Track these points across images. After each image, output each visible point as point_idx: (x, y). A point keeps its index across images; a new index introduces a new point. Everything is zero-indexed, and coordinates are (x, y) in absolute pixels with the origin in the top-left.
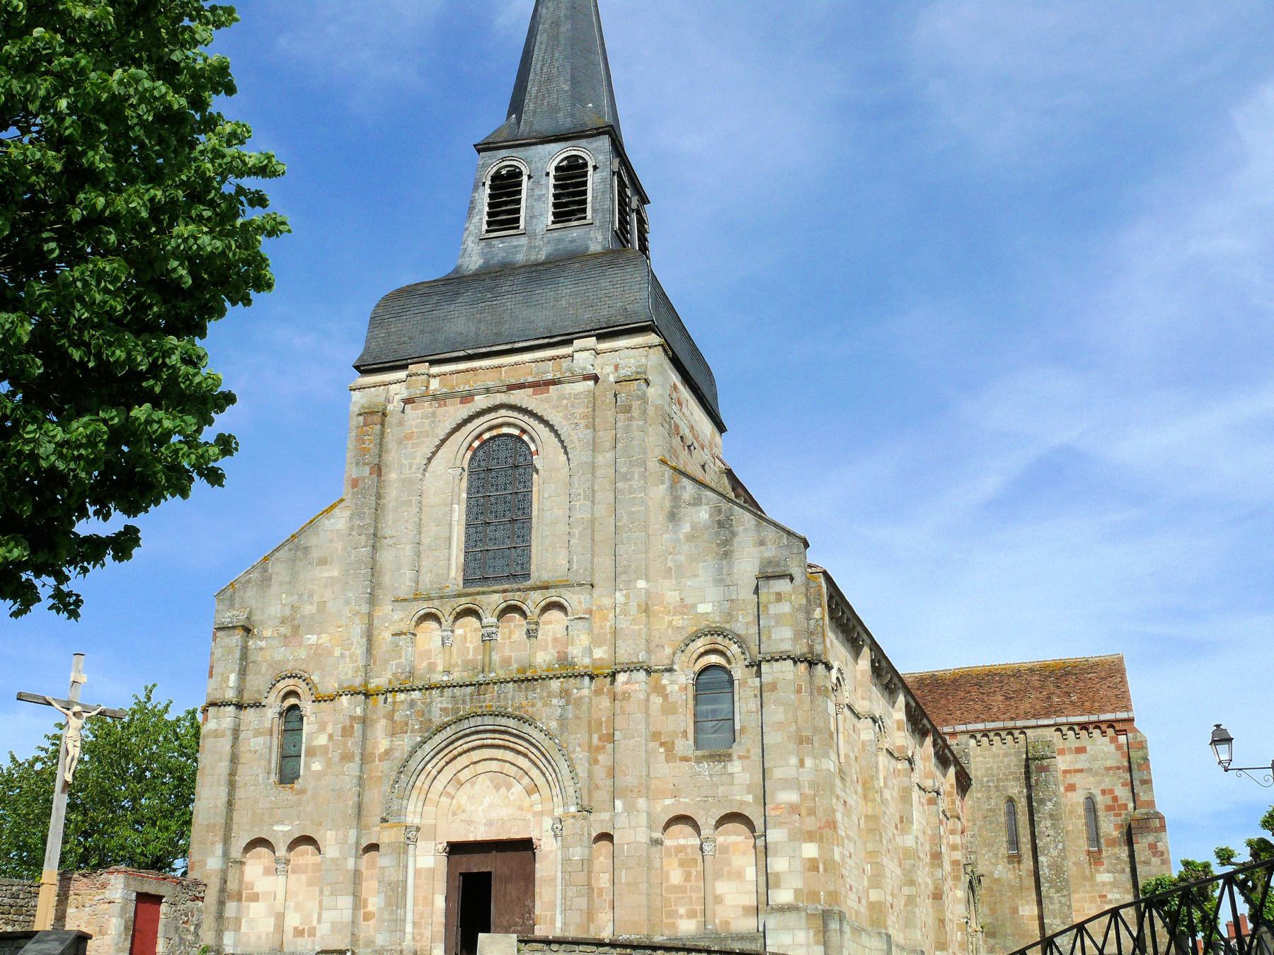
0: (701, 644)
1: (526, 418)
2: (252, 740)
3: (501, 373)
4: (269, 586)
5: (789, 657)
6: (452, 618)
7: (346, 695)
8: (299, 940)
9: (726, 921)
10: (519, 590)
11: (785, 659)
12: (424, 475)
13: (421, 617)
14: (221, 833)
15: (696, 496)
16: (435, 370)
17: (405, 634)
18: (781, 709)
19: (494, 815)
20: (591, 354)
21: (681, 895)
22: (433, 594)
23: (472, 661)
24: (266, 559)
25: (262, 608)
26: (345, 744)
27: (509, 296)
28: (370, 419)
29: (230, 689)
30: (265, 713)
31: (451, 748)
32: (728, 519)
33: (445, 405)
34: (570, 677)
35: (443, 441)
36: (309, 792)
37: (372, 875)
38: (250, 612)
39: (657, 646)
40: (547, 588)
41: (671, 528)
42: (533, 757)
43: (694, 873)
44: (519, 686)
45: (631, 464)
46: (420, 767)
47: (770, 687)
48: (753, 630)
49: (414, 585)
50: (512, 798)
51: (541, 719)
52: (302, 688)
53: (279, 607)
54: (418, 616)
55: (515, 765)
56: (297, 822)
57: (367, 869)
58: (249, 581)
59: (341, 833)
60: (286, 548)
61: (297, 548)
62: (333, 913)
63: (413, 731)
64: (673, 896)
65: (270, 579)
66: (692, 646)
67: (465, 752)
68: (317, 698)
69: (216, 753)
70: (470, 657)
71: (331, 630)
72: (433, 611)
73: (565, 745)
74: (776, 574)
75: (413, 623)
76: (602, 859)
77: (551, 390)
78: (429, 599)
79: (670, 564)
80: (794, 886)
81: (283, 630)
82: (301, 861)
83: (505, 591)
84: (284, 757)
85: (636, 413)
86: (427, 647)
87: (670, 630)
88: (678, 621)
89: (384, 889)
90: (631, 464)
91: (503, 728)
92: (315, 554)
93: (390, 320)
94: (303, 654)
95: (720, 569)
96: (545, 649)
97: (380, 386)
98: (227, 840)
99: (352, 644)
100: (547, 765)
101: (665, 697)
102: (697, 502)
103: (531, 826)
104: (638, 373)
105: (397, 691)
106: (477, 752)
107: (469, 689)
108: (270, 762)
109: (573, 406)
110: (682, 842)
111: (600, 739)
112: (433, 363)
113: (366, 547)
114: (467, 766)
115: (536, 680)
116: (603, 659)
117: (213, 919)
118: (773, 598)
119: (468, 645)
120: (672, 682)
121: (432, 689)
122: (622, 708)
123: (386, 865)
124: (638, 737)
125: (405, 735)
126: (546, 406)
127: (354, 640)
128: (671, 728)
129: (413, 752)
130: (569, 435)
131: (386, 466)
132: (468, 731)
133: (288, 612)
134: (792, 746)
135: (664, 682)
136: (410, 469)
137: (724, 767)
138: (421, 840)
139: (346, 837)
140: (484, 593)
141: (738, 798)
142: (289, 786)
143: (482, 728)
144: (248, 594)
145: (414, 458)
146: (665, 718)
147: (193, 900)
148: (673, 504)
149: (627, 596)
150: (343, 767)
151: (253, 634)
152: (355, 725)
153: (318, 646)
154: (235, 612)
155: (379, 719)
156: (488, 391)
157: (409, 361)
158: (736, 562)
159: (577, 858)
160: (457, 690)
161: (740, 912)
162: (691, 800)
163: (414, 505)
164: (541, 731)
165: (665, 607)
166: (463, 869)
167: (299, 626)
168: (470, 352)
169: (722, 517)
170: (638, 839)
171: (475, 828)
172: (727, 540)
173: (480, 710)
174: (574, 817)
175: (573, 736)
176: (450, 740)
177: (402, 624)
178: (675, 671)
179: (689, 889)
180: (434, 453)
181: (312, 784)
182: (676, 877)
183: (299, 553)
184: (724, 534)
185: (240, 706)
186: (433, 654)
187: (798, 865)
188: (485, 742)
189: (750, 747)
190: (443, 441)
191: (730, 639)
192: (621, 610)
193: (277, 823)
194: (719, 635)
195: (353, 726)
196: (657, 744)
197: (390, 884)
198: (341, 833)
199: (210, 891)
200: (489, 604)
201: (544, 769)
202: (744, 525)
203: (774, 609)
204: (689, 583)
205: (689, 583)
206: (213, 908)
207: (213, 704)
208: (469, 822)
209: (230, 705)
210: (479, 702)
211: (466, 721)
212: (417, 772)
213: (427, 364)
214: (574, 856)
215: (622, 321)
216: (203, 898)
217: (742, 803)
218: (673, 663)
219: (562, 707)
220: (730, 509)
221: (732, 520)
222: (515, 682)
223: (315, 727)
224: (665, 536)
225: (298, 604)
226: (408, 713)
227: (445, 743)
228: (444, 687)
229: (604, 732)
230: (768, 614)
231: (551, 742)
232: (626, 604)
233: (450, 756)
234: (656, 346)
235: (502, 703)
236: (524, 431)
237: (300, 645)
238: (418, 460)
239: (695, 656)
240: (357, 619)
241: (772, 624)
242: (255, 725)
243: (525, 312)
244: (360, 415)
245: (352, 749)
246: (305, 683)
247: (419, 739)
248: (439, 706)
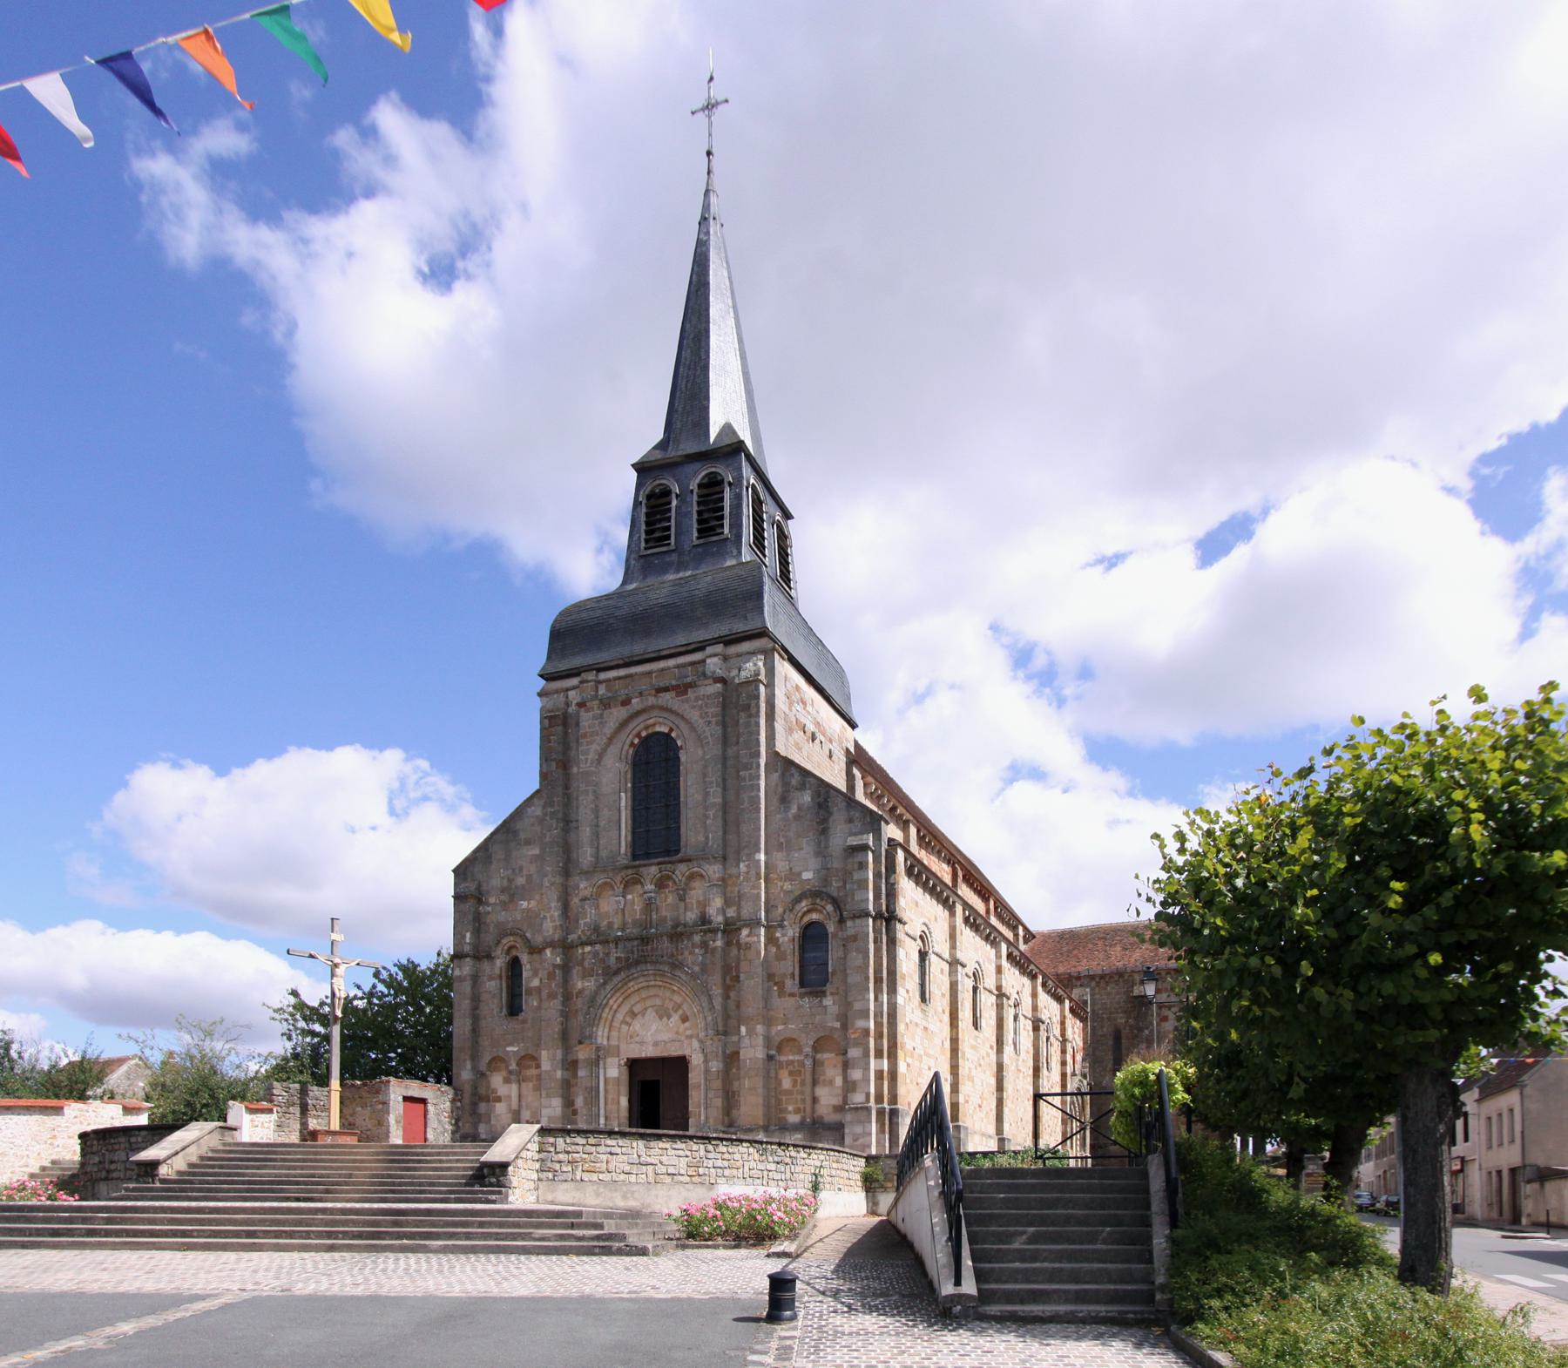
63: (597, 975)
66: (798, 908)
79: (782, 840)
81: (502, 897)
88: (787, 886)
92: (522, 836)
101: (778, 947)
107: (636, 943)
110: (791, 1058)
118: (856, 866)
120: (783, 935)
127: (553, 905)
133: (505, 883)
137: (821, 1001)
139: (554, 1055)
141: (830, 1024)
144: (476, 870)
149: (748, 866)
153: (528, 910)
184: (1040, 661)
223: (531, 973)
232: (747, 873)
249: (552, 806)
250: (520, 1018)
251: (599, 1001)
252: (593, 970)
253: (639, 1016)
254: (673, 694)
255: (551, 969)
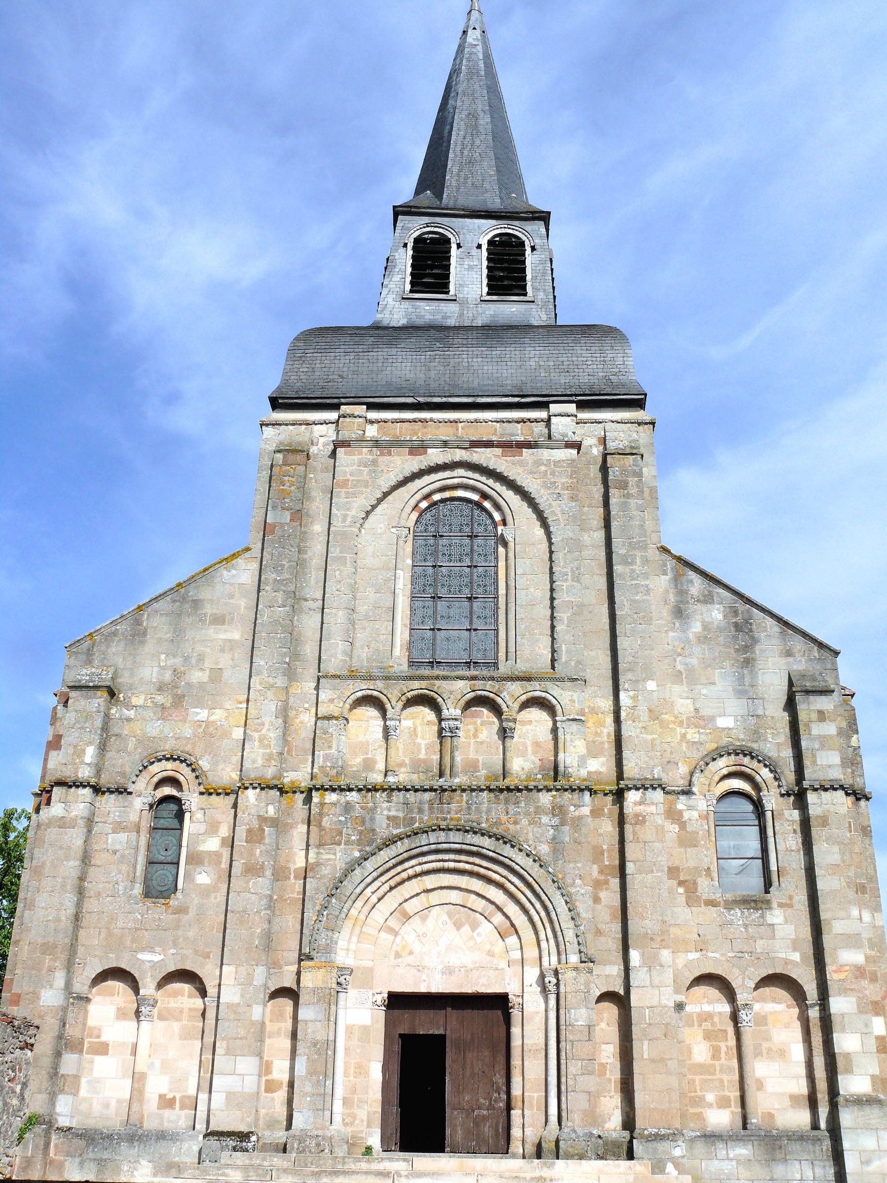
0: (723, 765)
1: (491, 482)
2: (110, 836)
3: (457, 429)
4: (142, 643)
5: (842, 787)
6: (400, 704)
7: (254, 788)
8: (167, 1113)
9: (769, 1113)
10: (492, 679)
11: (835, 789)
12: (360, 531)
13: (357, 699)
14: (64, 957)
15: (706, 592)
16: (373, 415)
17: (337, 718)
18: (836, 849)
19: (455, 960)
20: (572, 420)
21: (710, 1077)
22: (376, 672)
23: (425, 761)
24: (140, 608)
25: (132, 669)
26: (251, 853)
27: (464, 349)
28: (291, 457)
29: (86, 766)
30: (131, 803)
31: (399, 869)
32: (747, 622)
33: (390, 454)
34: (566, 790)
35: (386, 495)
36: (192, 913)
37: (280, 1029)
38: (115, 672)
39: (669, 762)
40: (528, 679)
41: (677, 625)
42: (512, 888)
43: (724, 1049)
44: (496, 796)
45: (632, 546)
46: (358, 890)
47: (820, 821)
48: (787, 753)
49: (348, 659)
50: (479, 940)
51: (527, 841)
52: (184, 774)
53: (156, 669)
54: (353, 697)
55: (483, 897)
56: (172, 951)
57: (271, 1021)
58: (115, 634)
59: (243, 970)
60: (168, 598)
61: (184, 599)
62: (230, 1079)
63: (348, 843)
64: (698, 1078)
65: (144, 634)
66: (713, 766)
67: (416, 876)
68: (207, 789)
69: (61, 848)
70: (422, 756)
71: (227, 705)
72: (375, 693)
73: (560, 876)
74: (818, 689)
75: (347, 706)
76: (603, 1025)
77: (524, 454)
78: (370, 678)
79: (679, 667)
80: (871, 1072)
81: (160, 699)
82: (173, 1003)
83: (474, 678)
84: (151, 862)
85: (633, 491)
86: (361, 738)
87: (684, 745)
88: (693, 735)
89: (307, 1051)
90: (632, 546)
91: (475, 849)
92: (209, 609)
93: (315, 355)
94: (188, 732)
95: (741, 678)
96: (523, 754)
97: (301, 424)
98: (69, 966)
99: (263, 724)
100: (533, 900)
101: (683, 825)
102: (707, 599)
103: (507, 978)
104: (632, 447)
105: (326, 790)
106: (432, 877)
107: (427, 796)
108: (135, 867)
109: (553, 474)
110: (707, 1008)
111: (601, 872)
112: (371, 406)
113: (284, 606)
114: (418, 894)
115: (519, 790)
116: (600, 773)
117: (46, 1076)
118: (814, 716)
119: (419, 740)
120: (690, 808)
121: (376, 790)
122: (634, 833)
123: (309, 1018)
124: (658, 871)
125: (338, 848)
126: (520, 470)
127: (267, 720)
128: (692, 864)
129: (349, 870)
130: (550, 505)
131: (308, 515)
132: (425, 849)
133: (168, 676)
134: (851, 894)
135: (680, 806)
136: (344, 520)
137: (762, 916)
138: (354, 987)
139: (250, 977)
140: (445, 678)
141: (783, 955)
142: (163, 901)
143: (445, 846)
144: (113, 649)
145: (348, 509)
146: (683, 850)
147: (22, 1049)
148: (678, 598)
149: (634, 698)
150: (248, 882)
151: (118, 700)
152: (266, 829)
153: (208, 723)
154: (93, 670)
155: (297, 823)
156: (445, 444)
157: (343, 400)
158: (760, 672)
159: (580, 1023)
160: (410, 796)
161: (787, 1102)
162: (722, 955)
163: (348, 564)
164: (528, 855)
165: (676, 717)
166: (404, 1029)
167: (184, 696)
168: (421, 400)
169: (739, 619)
170: (664, 1002)
171: (428, 976)
172: (746, 646)
173: (445, 823)
174: (576, 969)
175: (571, 865)
176: (401, 858)
177: (332, 706)
178: (693, 794)
179: (718, 1068)
180: (374, 507)
181: (196, 902)
182: (701, 1052)
183: (186, 606)
184: (742, 640)
185: (97, 790)
186: (371, 747)
187: (872, 1045)
188: (446, 865)
189: (792, 894)
190: (386, 495)
191: (759, 761)
192: (627, 714)
193: (143, 950)
194: (745, 755)
195: (263, 830)
196: (674, 883)
197: (315, 1045)
198: (243, 970)
199: (44, 1036)
200: (451, 693)
201: (528, 905)
202: (766, 631)
203: (817, 729)
204: (704, 691)
205: (704, 691)
206: (47, 1061)
207: (61, 783)
208: (420, 968)
209: (85, 787)
210: (442, 812)
211: (425, 836)
212: (353, 897)
213: (365, 407)
214: (577, 1021)
215: (608, 390)
216: (32, 1045)
217: (787, 962)
218: (690, 784)
219: (556, 828)
220: (748, 611)
221: (751, 624)
222: (491, 790)
223: (202, 828)
224: (671, 634)
225: (183, 669)
226: (342, 819)
227: (394, 861)
228: (393, 790)
229: (607, 863)
230: (810, 734)
231: (542, 870)
232: (634, 708)
233: (398, 879)
234: (646, 424)
235: (473, 817)
236: (485, 496)
237: (184, 720)
238: (353, 512)
239: (717, 778)
240: (270, 694)
241: (817, 746)
242: (115, 816)
243: (485, 368)
244: (279, 451)
245: (260, 860)
246: (189, 769)
247: (357, 854)
248: (385, 813)
249: (279, 573)
250: (173, 902)
251: (350, 888)
252: (340, 833)
253: (416, 920)
254: (498, 451)
255: (255, 824)
